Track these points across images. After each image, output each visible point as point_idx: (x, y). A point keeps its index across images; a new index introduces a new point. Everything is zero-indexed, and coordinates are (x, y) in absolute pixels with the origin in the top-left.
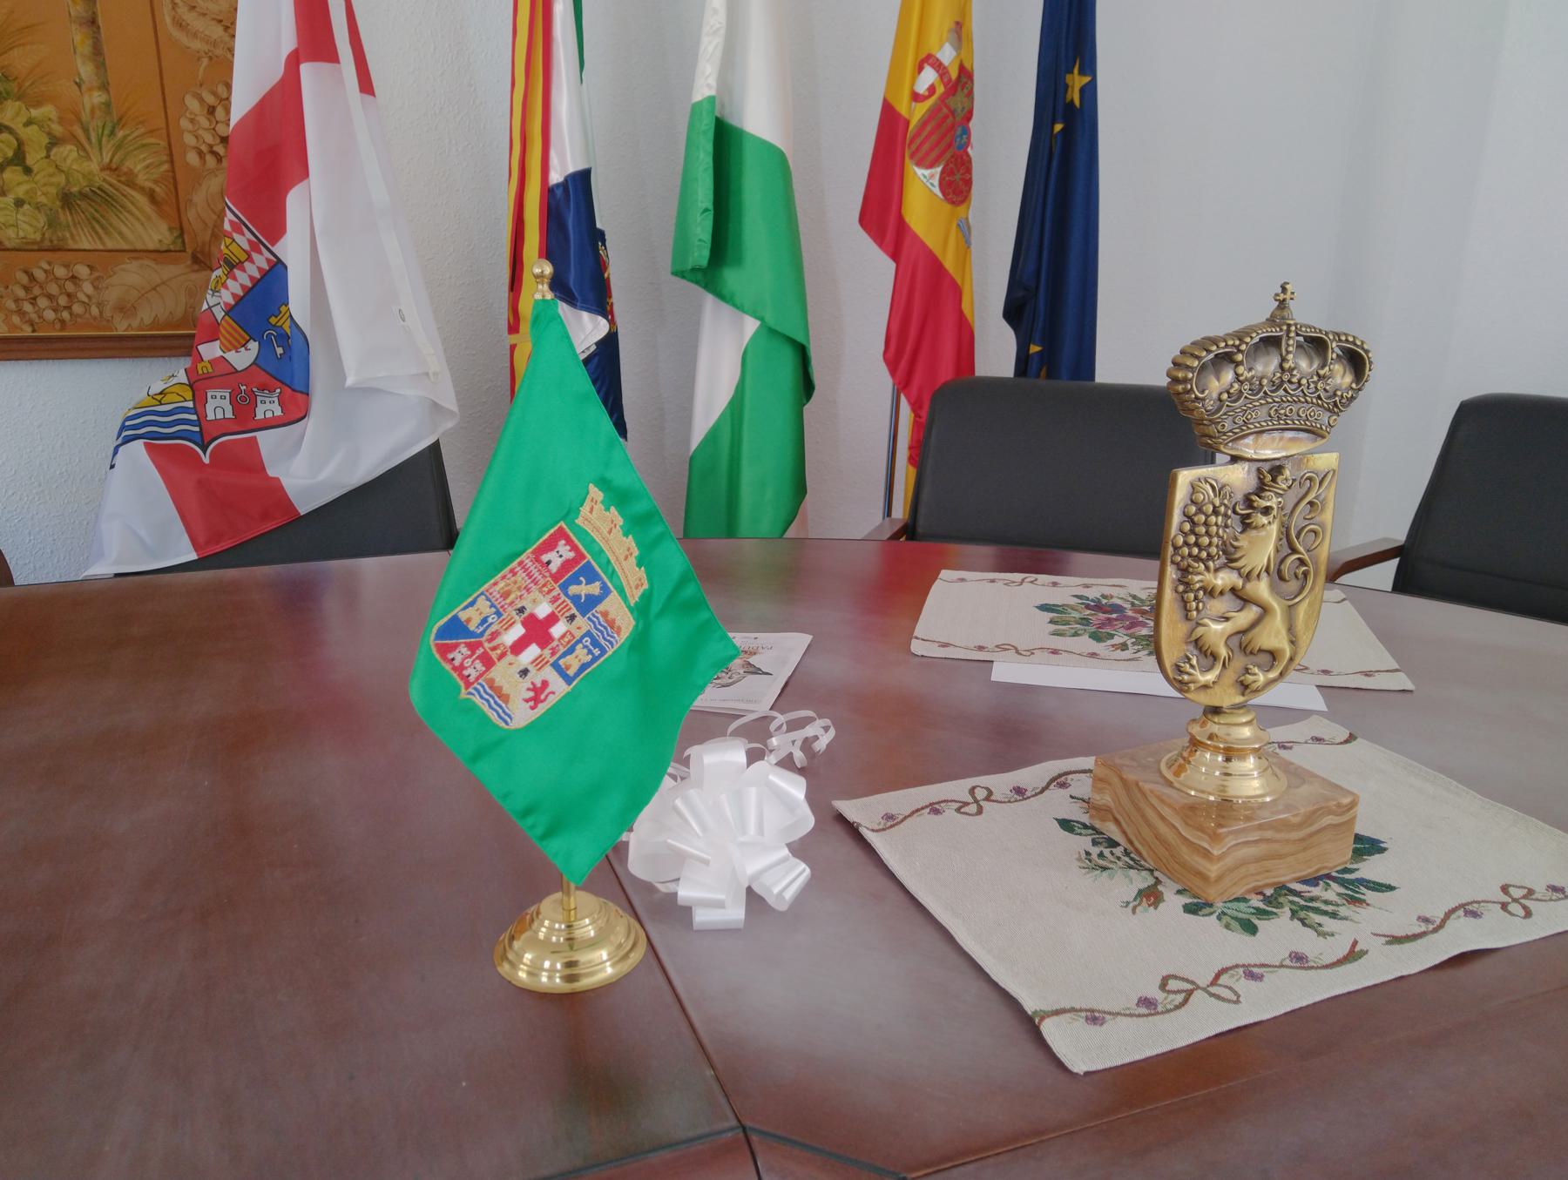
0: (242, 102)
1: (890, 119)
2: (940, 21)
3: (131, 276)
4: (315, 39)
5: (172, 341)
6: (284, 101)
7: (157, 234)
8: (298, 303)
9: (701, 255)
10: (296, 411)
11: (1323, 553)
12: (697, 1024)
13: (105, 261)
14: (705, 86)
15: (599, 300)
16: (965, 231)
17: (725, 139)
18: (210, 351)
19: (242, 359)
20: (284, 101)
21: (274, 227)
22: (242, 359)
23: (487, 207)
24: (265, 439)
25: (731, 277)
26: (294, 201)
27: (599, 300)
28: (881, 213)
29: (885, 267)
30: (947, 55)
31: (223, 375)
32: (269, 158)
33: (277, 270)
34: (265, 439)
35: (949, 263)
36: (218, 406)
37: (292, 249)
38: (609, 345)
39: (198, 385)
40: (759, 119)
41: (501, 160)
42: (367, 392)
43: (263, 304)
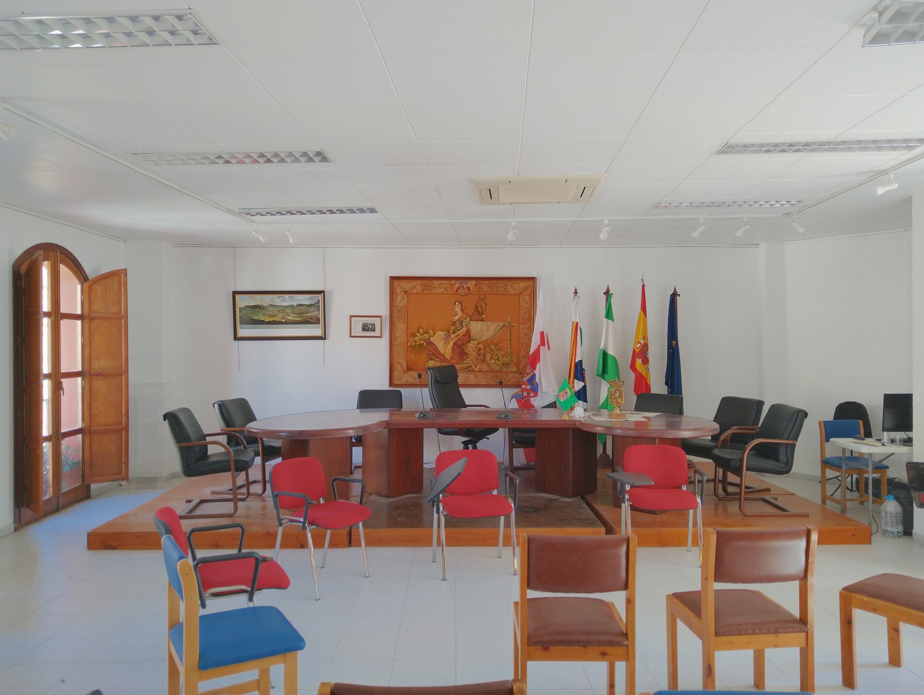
0: (532, 351)
1: (634, 351)
2: (641, 336)
3: (511, 375)
4: (542, 343)
5: (520, 386)
6: (537, 352)
7: (515, 369)
8: (537, 379)
9: (600, 373)
10: (536, 395)
11: (705, 478)
12: (258, 574)
13: (507, 373)
14: (602, 347)
15: (582, 379)
16: (648, 370)
17: (605, 354)
18: (524, 386)
19: (528, 388)
20: (537, 352)
21: (534, 368)
22: (528, 388)
23: (565, 366)
24: (531, 399)
25: (606, 376)
26: (538, 365)
27: (582, 379)
28: (633, 366)
29: (633, 375)
30: (642, 342)
31: (526, 390)
32: (535, 359)
33: (534, 375)
34: (531, 399)
35: (644, 374)
36: (525, 394)
37: (537, 372)
38: (585, 387)
39: (522, 391)
40: (611, 352)
41: (568, 358)
42: (546, 393)
43: (532, 379)
